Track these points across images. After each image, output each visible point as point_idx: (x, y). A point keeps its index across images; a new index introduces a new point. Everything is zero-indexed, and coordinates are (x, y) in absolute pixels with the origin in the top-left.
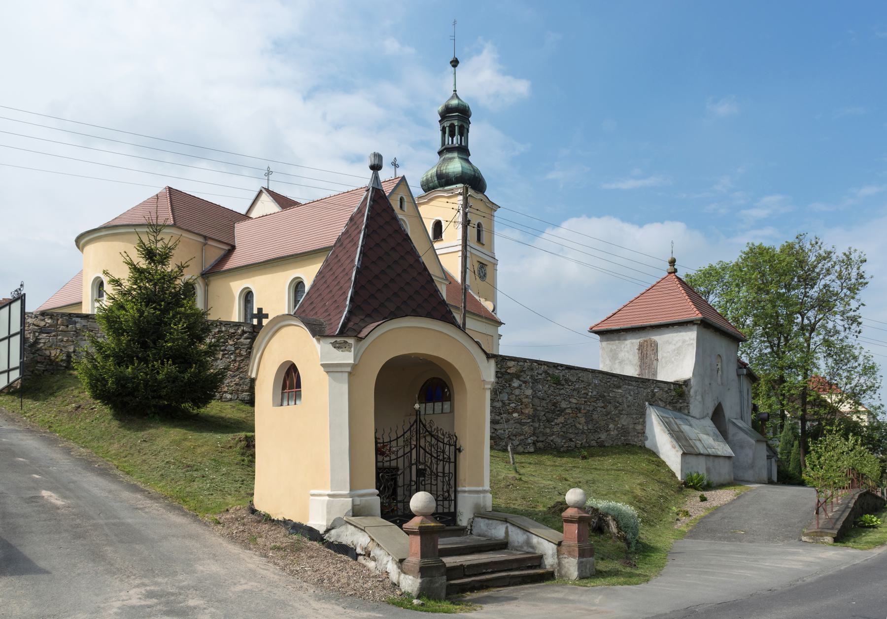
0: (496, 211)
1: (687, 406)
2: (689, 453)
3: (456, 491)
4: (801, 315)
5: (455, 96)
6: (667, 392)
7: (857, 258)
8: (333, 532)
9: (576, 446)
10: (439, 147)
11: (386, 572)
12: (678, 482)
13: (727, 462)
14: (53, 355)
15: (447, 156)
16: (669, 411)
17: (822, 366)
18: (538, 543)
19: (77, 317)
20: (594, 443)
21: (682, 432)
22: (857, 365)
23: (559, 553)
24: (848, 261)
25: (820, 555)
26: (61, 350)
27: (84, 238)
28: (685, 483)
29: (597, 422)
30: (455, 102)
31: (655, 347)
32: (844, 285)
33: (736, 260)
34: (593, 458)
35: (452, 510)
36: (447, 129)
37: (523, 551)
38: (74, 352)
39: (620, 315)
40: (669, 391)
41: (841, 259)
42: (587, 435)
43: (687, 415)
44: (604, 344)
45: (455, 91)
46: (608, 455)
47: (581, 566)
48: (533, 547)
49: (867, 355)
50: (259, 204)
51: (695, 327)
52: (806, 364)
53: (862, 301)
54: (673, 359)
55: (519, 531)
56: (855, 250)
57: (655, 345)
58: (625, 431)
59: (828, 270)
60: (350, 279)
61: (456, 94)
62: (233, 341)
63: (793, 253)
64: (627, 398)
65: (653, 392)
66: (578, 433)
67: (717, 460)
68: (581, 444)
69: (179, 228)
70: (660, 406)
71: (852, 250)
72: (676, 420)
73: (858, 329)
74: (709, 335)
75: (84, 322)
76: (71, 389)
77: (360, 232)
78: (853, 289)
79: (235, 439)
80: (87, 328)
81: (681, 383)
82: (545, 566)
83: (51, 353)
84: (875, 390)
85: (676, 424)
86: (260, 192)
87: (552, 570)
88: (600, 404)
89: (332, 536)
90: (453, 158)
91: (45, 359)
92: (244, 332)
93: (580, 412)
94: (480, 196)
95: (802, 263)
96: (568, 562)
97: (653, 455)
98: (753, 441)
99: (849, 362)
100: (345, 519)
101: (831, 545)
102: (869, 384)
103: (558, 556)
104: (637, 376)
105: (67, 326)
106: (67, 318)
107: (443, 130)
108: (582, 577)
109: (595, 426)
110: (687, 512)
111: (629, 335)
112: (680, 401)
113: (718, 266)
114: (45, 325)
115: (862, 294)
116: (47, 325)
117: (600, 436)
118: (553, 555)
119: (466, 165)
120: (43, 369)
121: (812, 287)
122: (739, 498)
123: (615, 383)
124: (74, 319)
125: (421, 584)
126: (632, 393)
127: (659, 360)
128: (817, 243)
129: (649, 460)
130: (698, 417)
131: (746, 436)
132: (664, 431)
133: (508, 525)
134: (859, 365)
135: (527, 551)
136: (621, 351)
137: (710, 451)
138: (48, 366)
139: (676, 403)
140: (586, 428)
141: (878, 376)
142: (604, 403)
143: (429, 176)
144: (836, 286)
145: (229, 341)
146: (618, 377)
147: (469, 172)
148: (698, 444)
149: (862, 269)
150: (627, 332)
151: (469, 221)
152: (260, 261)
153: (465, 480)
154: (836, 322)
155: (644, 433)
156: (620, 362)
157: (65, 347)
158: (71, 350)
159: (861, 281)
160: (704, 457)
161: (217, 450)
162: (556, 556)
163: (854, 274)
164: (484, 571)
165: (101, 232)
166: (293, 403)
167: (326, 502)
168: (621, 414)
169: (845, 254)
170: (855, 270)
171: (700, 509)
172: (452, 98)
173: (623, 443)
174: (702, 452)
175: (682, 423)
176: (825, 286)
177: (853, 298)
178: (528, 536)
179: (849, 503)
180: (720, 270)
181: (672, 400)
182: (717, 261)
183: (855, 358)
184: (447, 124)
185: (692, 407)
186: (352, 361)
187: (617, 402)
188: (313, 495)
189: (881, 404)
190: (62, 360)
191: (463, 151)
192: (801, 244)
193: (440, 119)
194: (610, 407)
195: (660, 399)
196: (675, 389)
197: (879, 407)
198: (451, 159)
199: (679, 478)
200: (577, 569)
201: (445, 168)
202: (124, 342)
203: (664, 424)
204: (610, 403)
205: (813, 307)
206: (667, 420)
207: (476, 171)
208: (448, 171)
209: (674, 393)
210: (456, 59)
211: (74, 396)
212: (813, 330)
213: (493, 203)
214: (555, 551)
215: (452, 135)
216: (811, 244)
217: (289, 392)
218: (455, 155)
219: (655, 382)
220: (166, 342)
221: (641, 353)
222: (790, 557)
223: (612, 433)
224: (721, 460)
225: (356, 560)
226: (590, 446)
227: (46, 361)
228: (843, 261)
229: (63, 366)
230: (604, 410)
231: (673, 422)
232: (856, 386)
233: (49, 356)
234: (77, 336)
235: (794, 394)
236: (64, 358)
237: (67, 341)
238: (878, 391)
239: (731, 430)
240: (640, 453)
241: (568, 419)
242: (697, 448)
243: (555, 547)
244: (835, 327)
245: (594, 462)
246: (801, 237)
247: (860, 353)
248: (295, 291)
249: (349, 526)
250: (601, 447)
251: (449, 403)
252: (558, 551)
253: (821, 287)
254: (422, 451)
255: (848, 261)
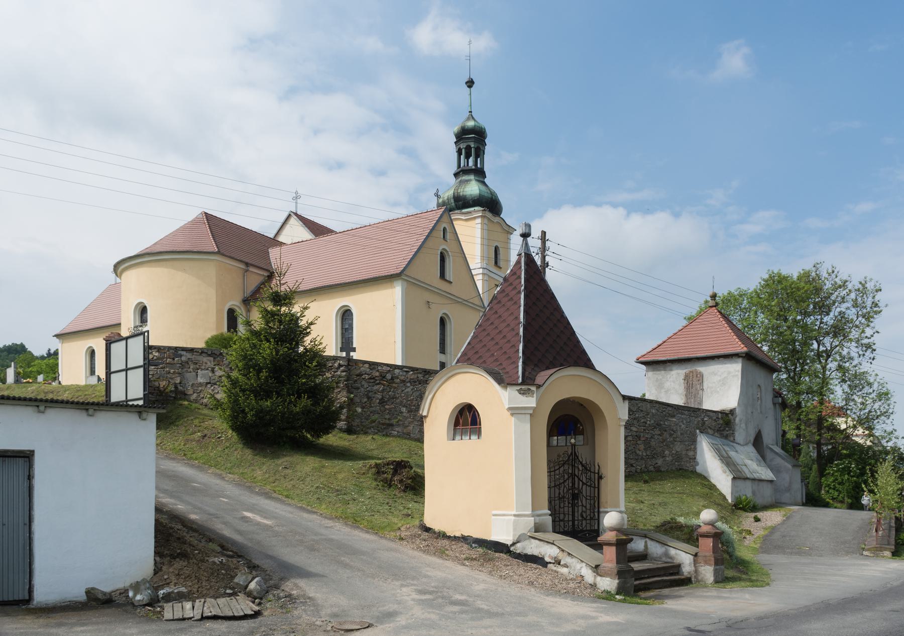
0: (512, 234)
1: (733, 434)
2: (738, 477)
3: (599, 512)
4: (817, 342)
5: (471, 117)
6: (715, 420)
7: (872, 288)
8: (518, 545)
9: (636, 471)
10: (454, 169)
11: (581, 576)
12: (730, 505)
13: (769, 485)
14: (162, 386)
15: (464, 178)
16: (717, 438)
17: (838, 393)
18: (676, 554)
19: (182, 350)
20: (651, 468)
21: (730, 458)
22: (871, 391)
23: (695, 562)
24: (863, 290)
25: (887, 566)
26: (169, 381)
27: (124, 263)
28: (735, 505)
29: (655, 449)
30: (471, 124)
31: (700, 377)
32: (860, 313)
33: (755, 287)
34: (653, 483)
35: (596, 528)
36: (463, 151)
37: (661, 561)
38: (180, 383)
39: (665, 346)
40: (717, 420)
41: (856, 288)
42: (646, 461)
43: (733, 442)
44: (650, 374)
45: (471, 112)
46: (666, 480)
47: (716, 572)
48: (671, 558)
49: (882, 382)
50: (287, 228)
51: (740, 360)
52: (822, 389)
53: (876, 329)
54: (718, 389)
55: (657, 545)
56: (871, 280)
57: (700, 376)
58: (678, 457)
59: (843, 298)
60: (518, 334)
61: (472, 115)
62: (331, 374)
63: (809, 281)
64: (680, 426)
65: (703, 420)
66: (638, 459)
67: (761, 484)
68: (641, 469)
69: (223, 255)
70: (709, 434)
71: (868, 279)
72: (724, 447)
73: (872, 356)
74: (752, 367)
75: (189, 355)
76: (190, 418)
77: (519, 292)
78: (868, 317)
79: (366, 466)
80: (192, 361)
81: (727, 412)
82: (683, 573)
83: (159, 384)
84: (889, 416)
85: (725, 451)
86: (289, 216)
87: (689, 576)
88: (657, 432)
89: (519, 548)
90: (470, 180)
91: (155, 390)
92: (340, 366)
93: (640, 440)
94: (496, 219)
95: (818, 290)
96: (704, 570)
97: (704, 479)
98: (790, 466)
99: (863, 388)
100: (528, 534)
101: (890, 558)
102: (883, 410)
103: (695, 564)
104: (683, 405)
105: (174, 359)
106: (174, 351)
107: (459, 152)
108: (717, 581)
109: (653, 453)
110: (750, 531)
111: (674, 367)
112: (727, 429)
113: (736, 293)
114: (153, 358)
115: (878, 322)
116: (155, 358)
117: (657, 461)
118: (690, 564)
119: (483, 188)
120: (154, 399)
121: (828, 314)
122: (788, 518)
123: (670, 412)
124: (180, 352)
125: (618, 584)
126: (685, 422)
127: (705, 390)
128: (833, 272)
129: (702, 484)
130: (742, 443)
131: (783, 461)
132: (714, 456)
133: (647, 539)
134: (874, 391)
135: (666, 561)
136: (667, 380)
137: (756, 476)
138: (158, 397)
139: (723, 430)
140: (645, 454)
141: (892, 402)
142: (660, 431)
143: (446, 198)
144: (852, 313)
145: (327, 374)
146: (672, 407)
147: (486, 195)
148: (744, 468)
149: (877, 298)
150: (672, 363)
151: (548, 263)
152: (306, 289)
153: (607, 502)
154: (851, 349)
155: (695, 458)
156: (665, 391)
157: (172, 379)
158: (178, 381)
159: (875, 309)
160: (750, 481)
161: (355, 476)
162: (693, 565)
163: (869, 303)
164: (643, 576)
165: (145, 257)
166: (468, 437)
167: (512, 521)
168: (676, 441)
169: (861, 283)
170: (870, 299)
171: (758, 529)
172: (468, 119)
173: (677, 468)
174: (749, 477)
175: (729, 450)
176: (840, 313)
177: (868, 326)
178: (666, 548)
179: (890, 523)
180: (738, 297)
181: (720, 428)
182: (736, 288)
183: (870, 385)
184: (463, 146)
185: (737, 434)
186: (534, 405)
187: (672, 431)
188: (494, 515)
189: (894, 429)
190: (171, 391)
191: (480, 173)
192: (818, 273)
193: (455, 140)
194: (666, 435)
195: (709, 427)
196: (722, 418)
197: (892, 432)
198: (468, 181)
199: (730, 501)
200: (713, 575)
201: (462, 190)
202: (263, 378)
203: (715, 450)
204: (666, 431)
205: (827, 334)
206: (717, 447)
207: (493, 194)
208: (465, 193)
209: (721, 422)
210: (472, 79)
211: (195, 426)
212: (828, 356)
213: (510, 226)
214: (692, 560)
215: (468, 157)
216: (827, 273)
217: (470, 428)
218: (472, 177)
219: (705, 411)
220: (299, 378)
221: (687, 384)
222: (863, 568)
223: (668, 459)
224: (765, 484)
225: (546, 567)
226: (649, 471)
227: (156, 392)
228: (859, 290)
229: (172, 397)
230: (661, 438)
231: (721, 448)
232: (870, 412)
233: (158, 387)
234: (182, 369)
235: (811, 419)
236: (173, 389)
237: (174, 373)
238: (892, 417)
239: (769, 455)
240: (693, 478)
241: (630, 446)
242: (745, 473)
243: (692, 557)
244: (849, 353)
245: (657, 486)
246: (818, 266)
247: (875, 380)
248: (342, 319)
249: (533, 540)
250: (658, 472)
251: (582, 436)
252: (694, 561)
253: (837, 314)
254: (576, 479)
255: (863, 290)
